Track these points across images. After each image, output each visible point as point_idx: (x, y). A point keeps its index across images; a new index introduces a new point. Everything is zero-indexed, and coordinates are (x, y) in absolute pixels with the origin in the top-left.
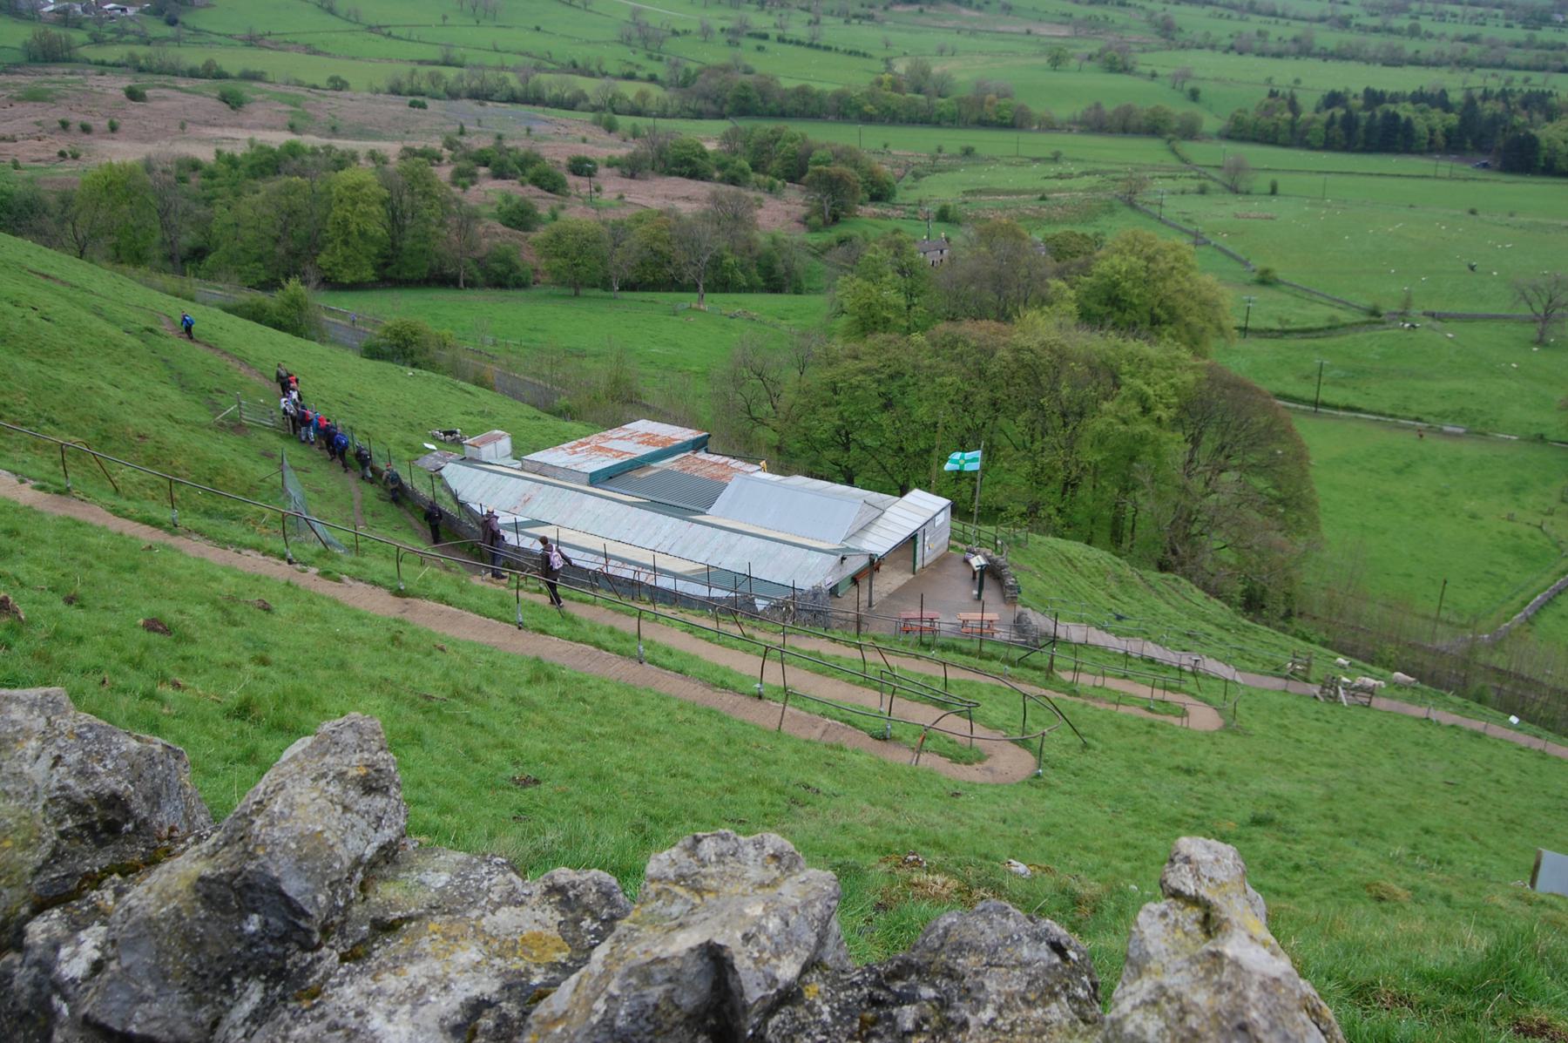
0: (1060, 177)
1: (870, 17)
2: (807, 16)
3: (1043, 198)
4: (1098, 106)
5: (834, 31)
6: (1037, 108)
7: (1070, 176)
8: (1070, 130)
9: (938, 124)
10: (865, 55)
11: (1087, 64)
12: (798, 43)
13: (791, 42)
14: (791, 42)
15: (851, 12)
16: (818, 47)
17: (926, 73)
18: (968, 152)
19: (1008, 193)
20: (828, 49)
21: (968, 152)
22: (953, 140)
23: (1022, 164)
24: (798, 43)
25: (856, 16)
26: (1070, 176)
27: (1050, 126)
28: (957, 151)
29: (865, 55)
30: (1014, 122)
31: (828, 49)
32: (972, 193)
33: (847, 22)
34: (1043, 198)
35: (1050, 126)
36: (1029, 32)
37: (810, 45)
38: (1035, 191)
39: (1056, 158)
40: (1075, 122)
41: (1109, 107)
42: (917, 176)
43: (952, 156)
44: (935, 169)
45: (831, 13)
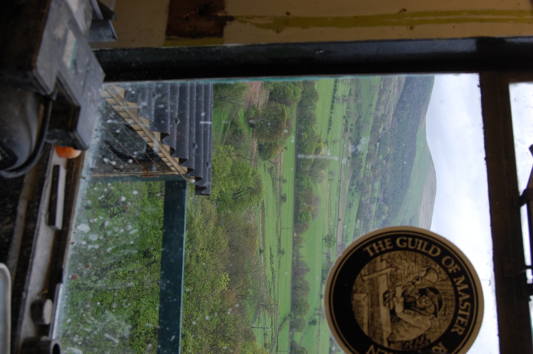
0: (272, 256)
1: (346, 130)
2: (347, 94)
3: (261, 251)
4: (308, 270)
5: (340, 109)
6: (305, 236)
7: (272, 263)
8: (293, 256)
9: (296, 177)
10: (329, 129)
11: (325, 256)
12: (335, 90)
13: (335, 86)
14: (335, 86)
15: (349, 119)
16: (333, 102)
17: (323, 167)
18: (283, 198)
19: (263, 228)
20: (332, 107)
21: (283, 198)
22: (288, 189)
23: (277, 232)
24: (335, 90)
25: (346, 122)
26: (272, 263)
27: (296, 243)
28: (283, 192)
29: (329, 129)
30: (299, 221)
31: (332, 107)
32: (263, 206)
33: (344, 117)
34: (261, 251)
35: (296, 243)
36: (339, 220)
37: (334, 97)
38: (264, 246)
39: (281, 252)
40: (298, 257)
41: (307, 277)
42: (271, 170)
43: (281, 189)
44: (274, 180)
45: (348, 108)
